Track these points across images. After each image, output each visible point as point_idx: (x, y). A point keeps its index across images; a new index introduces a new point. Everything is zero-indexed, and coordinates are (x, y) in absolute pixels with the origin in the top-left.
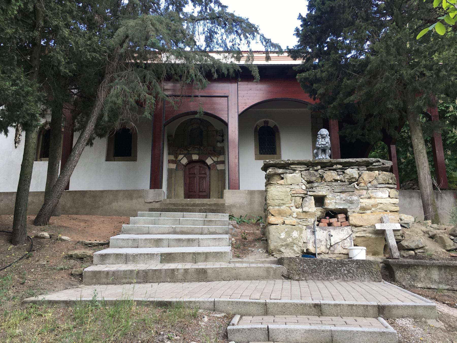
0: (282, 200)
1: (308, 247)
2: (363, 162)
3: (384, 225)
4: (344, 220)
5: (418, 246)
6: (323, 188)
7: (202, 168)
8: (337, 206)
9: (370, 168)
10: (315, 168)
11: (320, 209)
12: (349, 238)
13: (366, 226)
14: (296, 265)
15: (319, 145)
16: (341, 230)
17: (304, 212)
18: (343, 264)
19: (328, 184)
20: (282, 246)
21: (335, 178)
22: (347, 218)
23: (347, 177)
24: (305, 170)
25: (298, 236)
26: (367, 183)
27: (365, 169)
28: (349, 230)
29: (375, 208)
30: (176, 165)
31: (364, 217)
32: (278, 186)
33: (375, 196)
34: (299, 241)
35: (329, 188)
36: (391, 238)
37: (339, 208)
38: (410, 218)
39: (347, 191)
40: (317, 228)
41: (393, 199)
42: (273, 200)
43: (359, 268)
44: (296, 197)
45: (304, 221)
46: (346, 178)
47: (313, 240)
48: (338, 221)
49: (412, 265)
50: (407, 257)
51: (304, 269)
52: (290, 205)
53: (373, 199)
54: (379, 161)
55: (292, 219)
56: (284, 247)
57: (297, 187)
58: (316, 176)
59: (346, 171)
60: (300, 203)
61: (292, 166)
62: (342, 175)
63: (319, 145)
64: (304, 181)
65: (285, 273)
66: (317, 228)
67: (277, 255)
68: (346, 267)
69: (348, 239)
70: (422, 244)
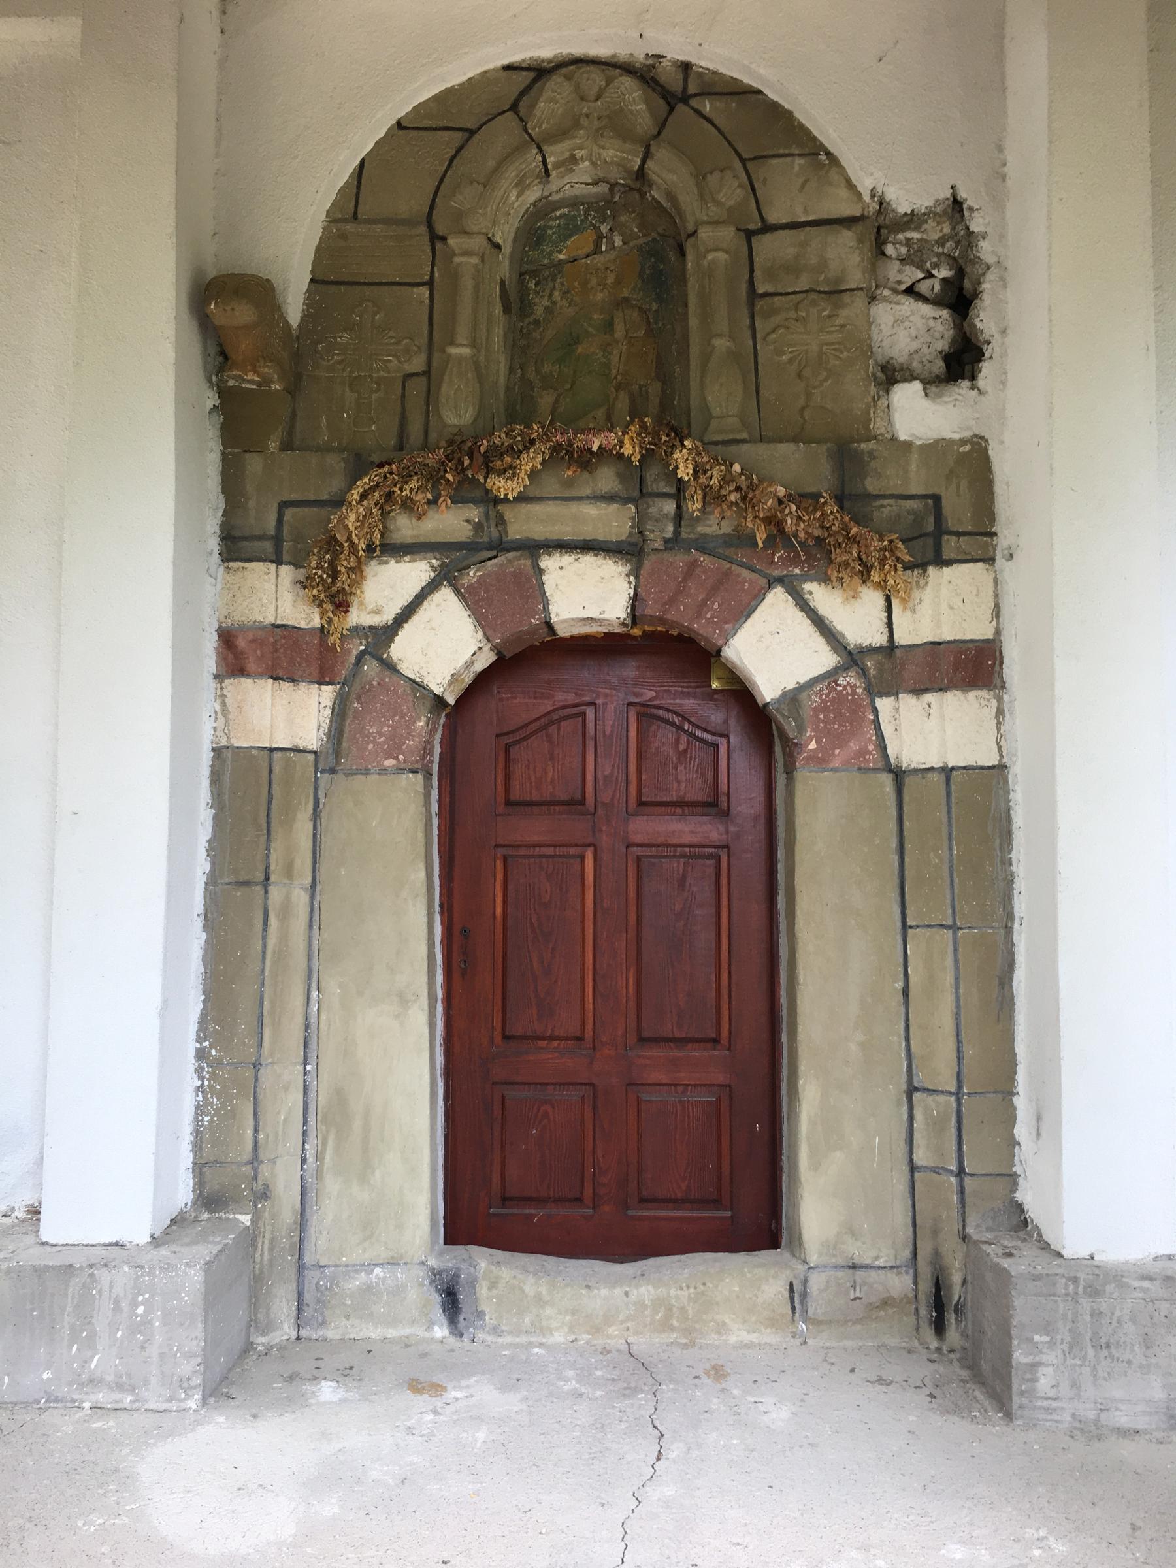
7: (666, 735)
30: (328, 693)
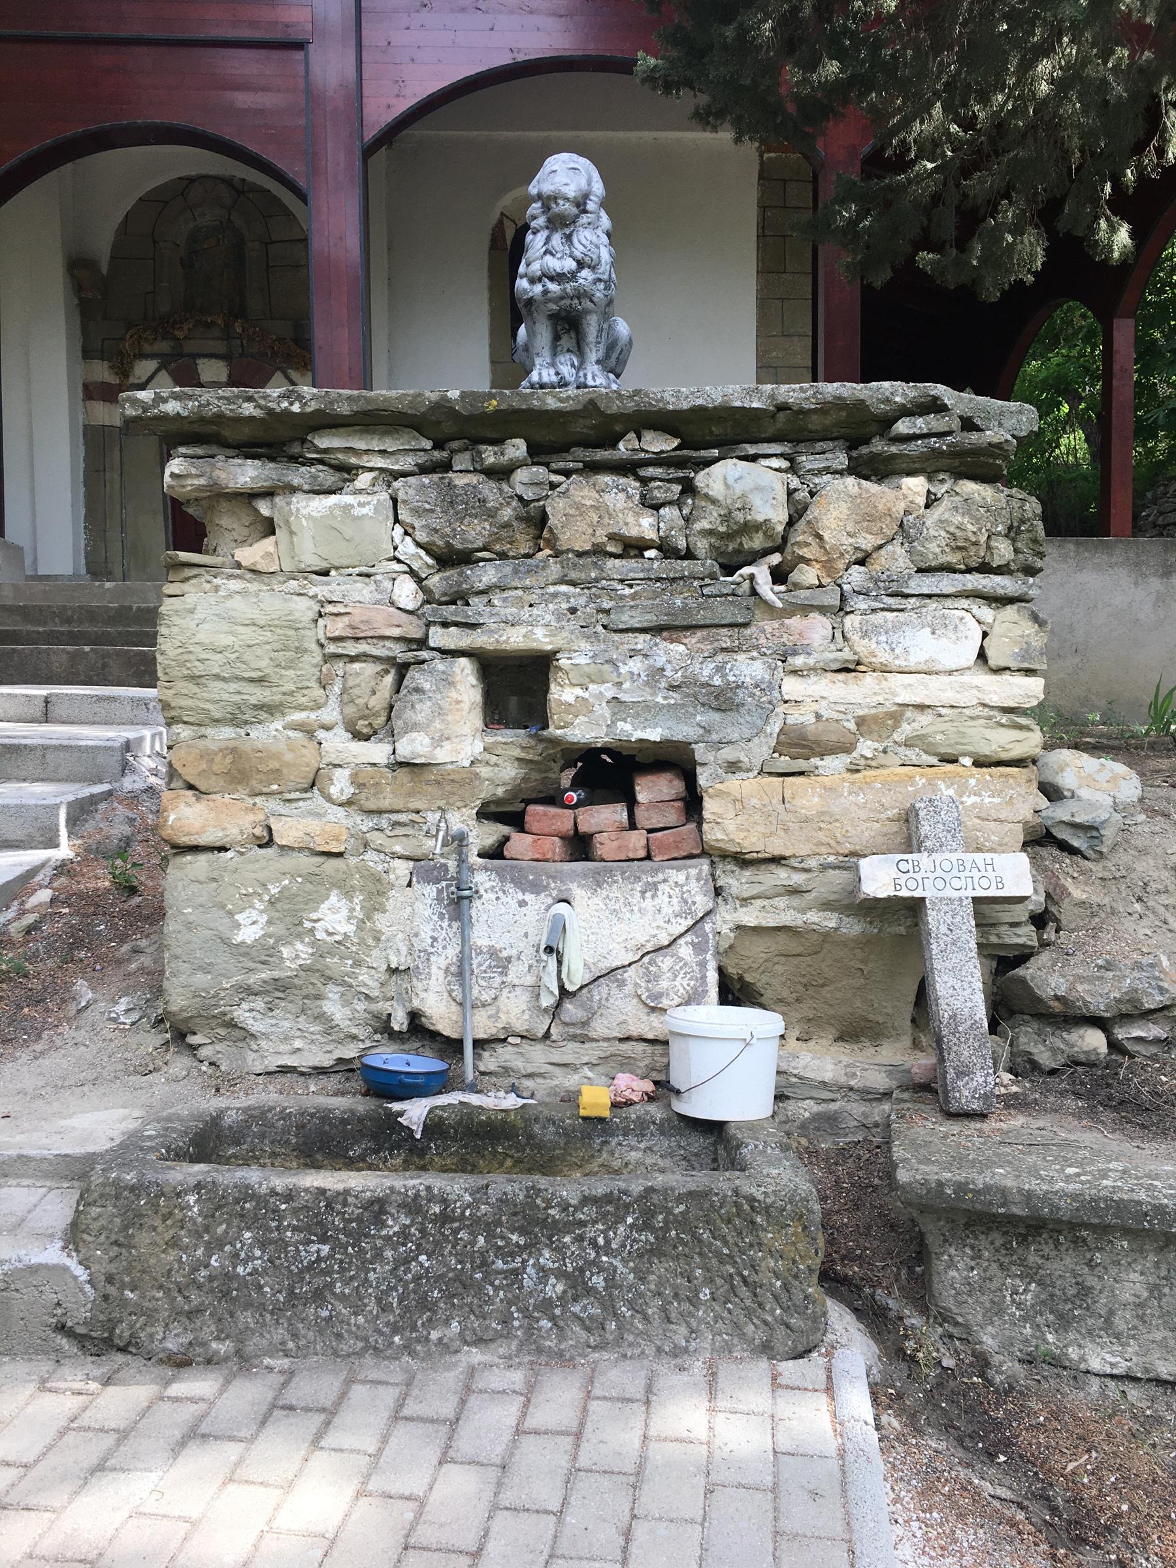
0: (260, 681)
1: (416, 1003)
2: (827, 408)
3: (916, 868)
4: (672, 815)
5: (1134, 1001)
6: (533, 598)
8: (627, 727)
9: (874, 457)
10: (490, 456)
11: (512, 740)
12: (688, 938)
13: (813, 863)
14: (174, 1243)
15: (532, 281)
16: (638, 887)
17: (401, 764)
18: (543, 1223)
19: (573, 575)
20: (249, 991)
21: (625, 531)
22: (692, 804)
23: (704, 524)
24: (423, 470)
25: (350, 928)
26: (841, 565)
27: (836, 465)
28: (694, 886)
29: (880, 739)
31: (798, 802)
32: (235, 585)
33: (883, 657)
34: (357, 963)
35: (578, 596)
36: (956, 958)
37: (641, 741)
38: (1114, 779)
39: (700, 617)
40: (483, 880)
41: (1006, 677)
42: (194, 678)
43: (654, 1252)
44: (353, 659)
45: (396, 824)
46: (698, 526)
47: (452, 952)
48: (632, 826)
49: (1060, 1221)
50: (1053, 1072)
51: (230, 1277)
52: (313, 716)
53: (869, 680)
54: (936, 407)
55: (319, 815)
56: (259, 1004)
57: (362, 591)
58: (491, 514)
59: (701, 479)
60: (378, 702)
61: (324, 442)
62: (678, 503)
63: (532, 281)
64: (408, 548)
65: (79, 1314)
66: (483, 880)
67: (218, 1047)
68: (559, 1250)
69: (684, 950)
70: (1162, 990)
